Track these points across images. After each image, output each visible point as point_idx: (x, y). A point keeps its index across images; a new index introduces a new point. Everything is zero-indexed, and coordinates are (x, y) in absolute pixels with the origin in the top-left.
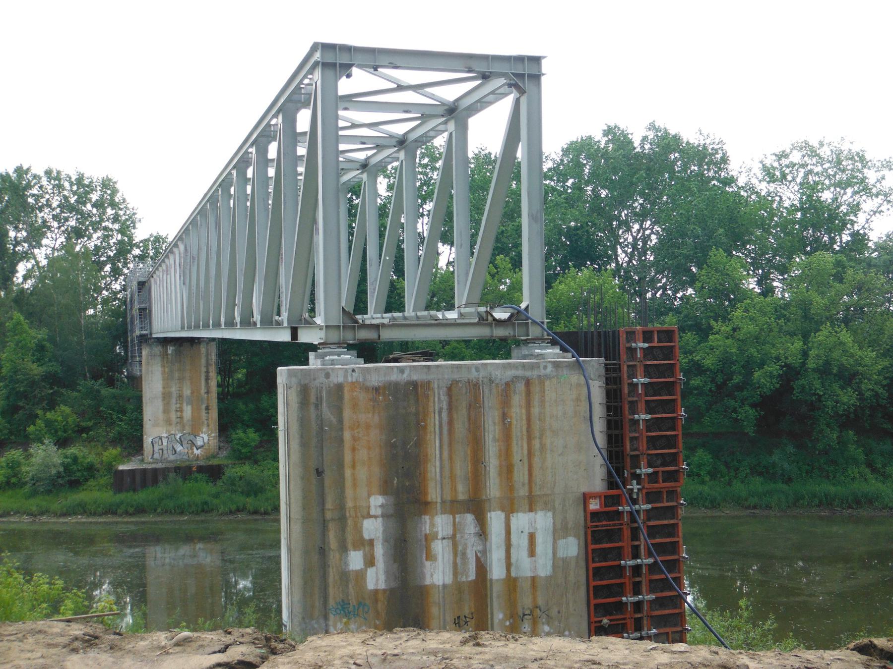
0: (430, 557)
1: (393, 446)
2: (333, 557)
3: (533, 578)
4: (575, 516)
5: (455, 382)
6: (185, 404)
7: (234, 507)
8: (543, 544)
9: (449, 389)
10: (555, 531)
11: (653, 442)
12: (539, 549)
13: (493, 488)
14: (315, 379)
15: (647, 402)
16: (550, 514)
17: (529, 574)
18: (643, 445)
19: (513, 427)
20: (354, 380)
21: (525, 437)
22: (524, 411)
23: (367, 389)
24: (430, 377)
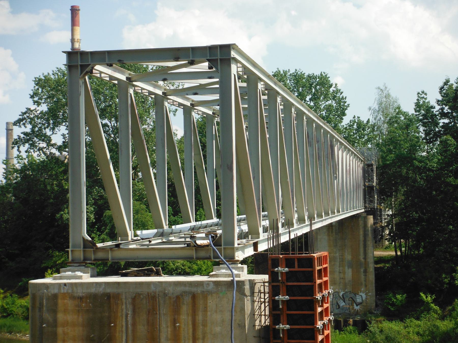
5: (139, 295)
6: (347, 268)
9: (134, 299)
14: (39, 290)
15: (288, 315)
19: (182, 329)
20: (65, 291)
21: (191, 338)
22: (190, 318)
23: (73, 298)
24: (120, 291)
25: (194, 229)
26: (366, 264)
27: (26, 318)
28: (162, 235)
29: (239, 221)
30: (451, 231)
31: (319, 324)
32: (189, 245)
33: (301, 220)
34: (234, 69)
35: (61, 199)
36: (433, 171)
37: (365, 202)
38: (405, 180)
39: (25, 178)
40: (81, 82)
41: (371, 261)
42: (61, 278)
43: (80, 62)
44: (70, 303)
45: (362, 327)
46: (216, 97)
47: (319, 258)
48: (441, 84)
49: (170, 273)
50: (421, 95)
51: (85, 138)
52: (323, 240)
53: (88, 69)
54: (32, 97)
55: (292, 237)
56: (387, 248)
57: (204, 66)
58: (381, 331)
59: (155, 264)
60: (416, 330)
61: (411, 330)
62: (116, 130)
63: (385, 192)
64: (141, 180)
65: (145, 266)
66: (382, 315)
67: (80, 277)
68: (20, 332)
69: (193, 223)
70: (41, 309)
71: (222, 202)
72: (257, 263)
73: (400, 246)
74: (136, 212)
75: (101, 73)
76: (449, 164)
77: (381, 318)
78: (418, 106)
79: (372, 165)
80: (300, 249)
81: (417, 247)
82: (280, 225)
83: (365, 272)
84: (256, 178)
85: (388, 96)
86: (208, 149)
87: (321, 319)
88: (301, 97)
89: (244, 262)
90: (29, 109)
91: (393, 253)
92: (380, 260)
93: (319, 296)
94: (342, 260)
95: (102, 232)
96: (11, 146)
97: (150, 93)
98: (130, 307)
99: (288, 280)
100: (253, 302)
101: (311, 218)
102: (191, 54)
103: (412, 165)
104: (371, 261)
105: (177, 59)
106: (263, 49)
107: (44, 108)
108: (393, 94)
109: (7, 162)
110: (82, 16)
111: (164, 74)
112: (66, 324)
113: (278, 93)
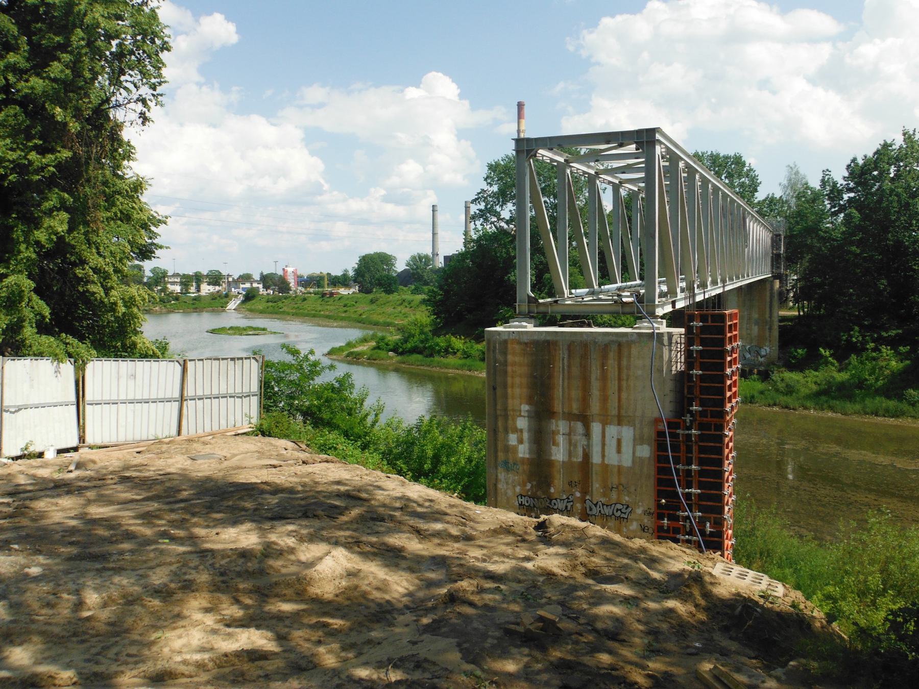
0: (555, 444)
1: (535, 377)
2: (501, 435)
3: (619, 466)
4: (649, 432)
7: (772, 402)
8: (627, 448)
9: (569, 346)
10: (634, 440)
11: (703, 390)
12: (624, 449)
13: (595, 406)
15: (701, 363)
16: (632, 428)
17: (616, 463)
18: (697, 391)
23: (519, 343)
25: (622, 289)
26: (771, 322)
27: (483, 360)
28: (592, 293)
29: (660, 283)
30: (851, 294)
31: (728, 371)
32: (616, 302)
33: (714, 283)
34: (658, 150)
35: (509, 264)
36: (837, 241)
37: (772, 268)
38: (810, 248)
39: (480, 246)
40: (526, 164)
41: (776, 320)
42: (510, 327)
43: (526, 147)
44: (517, 347)
45: (765, 376)
46: (642, 175)
47: (730, 315)
48: (849, 162)
49: (599, 325)
50: (826, 172)
51: (530, 214)
52: (733, 299)
53: (532, 153)
54: (486, 180)
55: (707, 297)
56: (791, 308)
57: (631, 148)
58: (782, 380)
59: (586, 317)
60: (814, 379)
61: (809, 379)
62: (554, 207)
63: (791, 259)
64: (575, 248)
65: (579, 319)
66: (783, 366)
67: (525, 327)
68: (477, 370)
69: (619, 284)
70: (494, 351)
71: (645, 268)
72: (675, 318)
73: (803, 307)
74: (571, 275)
75: (543, 156)
76: (853, 234)
77: (783, 369)
78: (824, 183)
79: (780, 235)
80: (714, 307)
81: (818, 308)
82: (696, 286)
83: (770, 329)
84: (676, 245)
85: (797, 173)
86: (633, 221)
87: (730, 367)
88: (718, 175)
89: (662, 317)
90: (483, 190)
91: (797, 313)
92: (783, 319)
93: (729, 348)
94: (749, 319)
95: (542, 292)
96: (469, 220)
97: (585, 173)
98: (566, 352)
99: (702, 333)
100: (671, 351)
101: (723, 281)
102: (620, 138)
103: (817, 235)
104: (776, 320)
105: (608, 143)
106: (684, 132)
107: (495, 188)
108: (802, 171)
109: (466, 233)
110: (526, 110)
111: (596, 156)
112: (514, 364)
113: (697, 171)
